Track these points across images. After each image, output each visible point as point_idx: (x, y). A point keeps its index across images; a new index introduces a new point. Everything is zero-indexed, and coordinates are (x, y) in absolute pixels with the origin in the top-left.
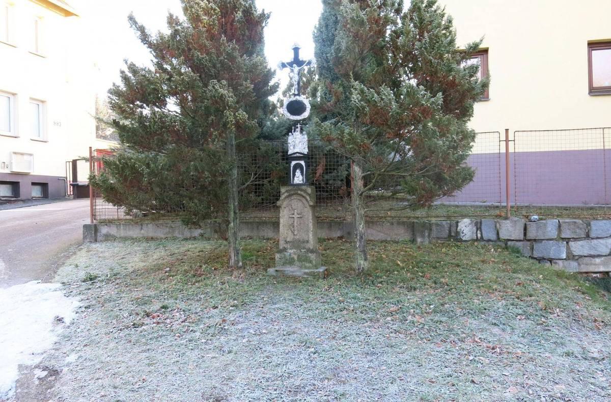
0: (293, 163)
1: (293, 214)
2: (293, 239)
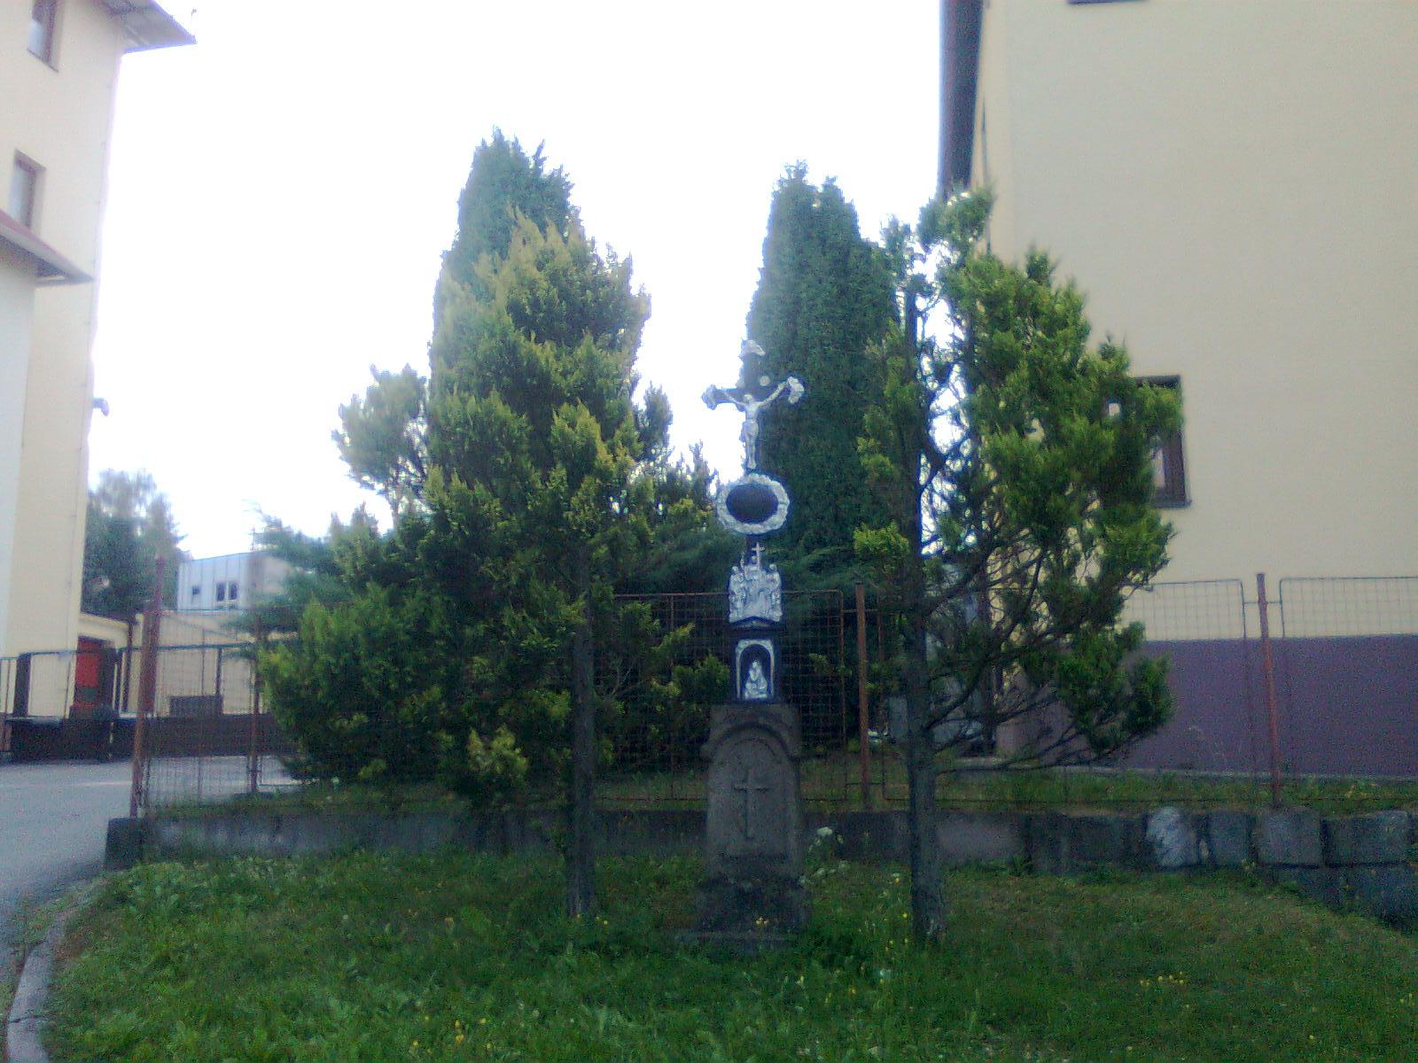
0: (743, 645)
1: (745, 781)
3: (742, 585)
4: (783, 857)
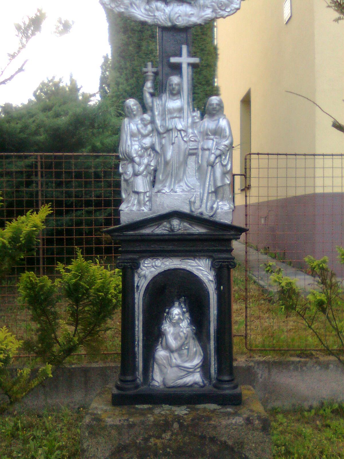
3: (147, 142)
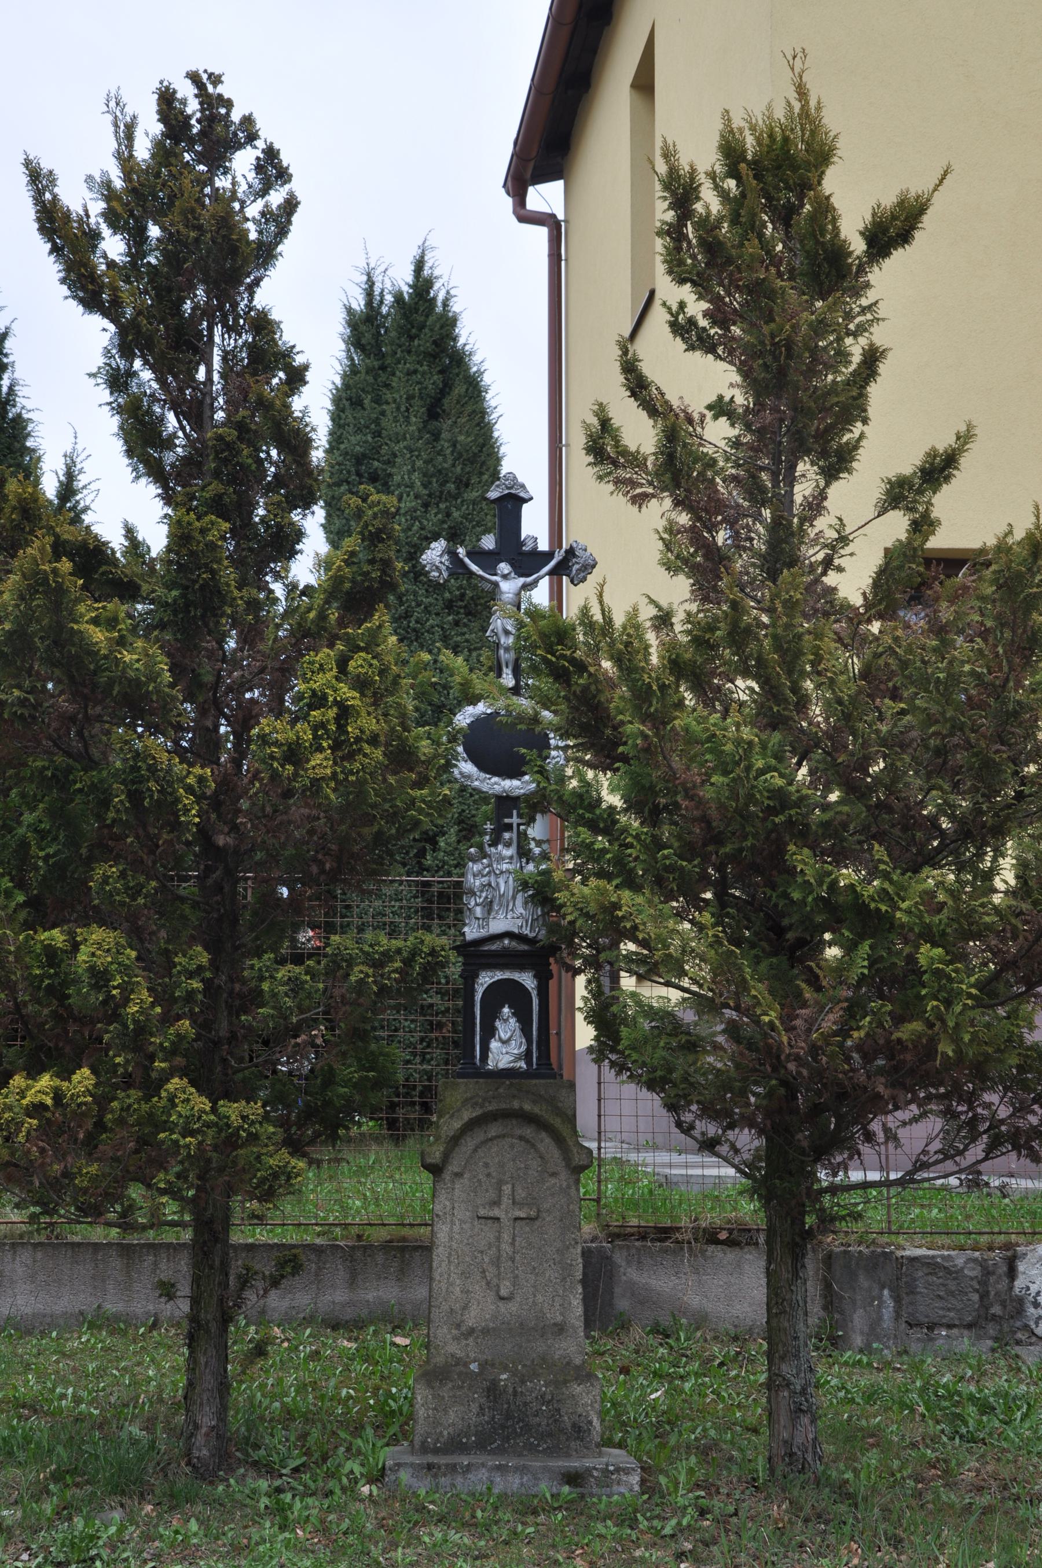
0: (485, 979)
1: (496, 1203)
2: (494, 1318)
4: (560, 1329)
